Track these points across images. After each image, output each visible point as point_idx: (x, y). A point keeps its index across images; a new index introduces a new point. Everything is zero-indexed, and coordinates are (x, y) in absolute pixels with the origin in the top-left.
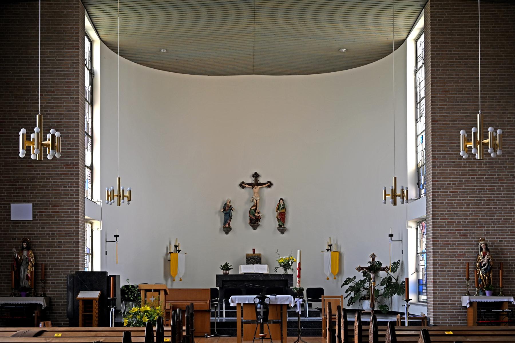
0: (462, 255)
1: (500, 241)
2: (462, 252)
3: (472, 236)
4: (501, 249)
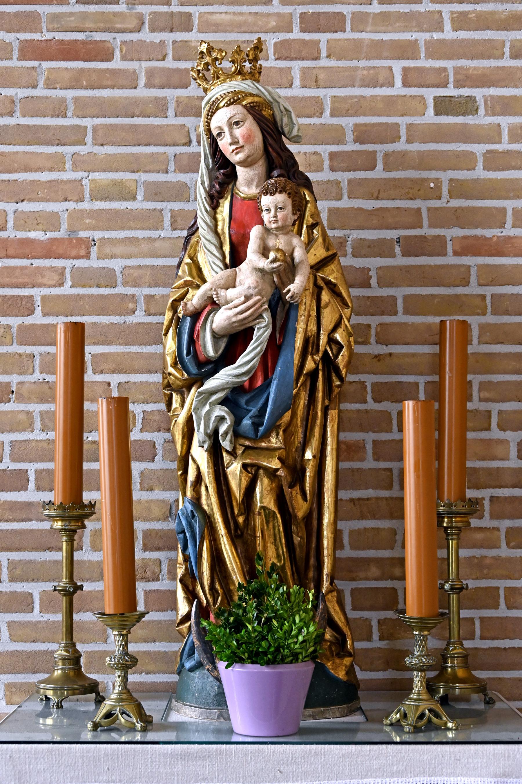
0: (49, 250)
1: (443, 106)
2: (51, 221)
3: (158, 52)
4: (458, 189)
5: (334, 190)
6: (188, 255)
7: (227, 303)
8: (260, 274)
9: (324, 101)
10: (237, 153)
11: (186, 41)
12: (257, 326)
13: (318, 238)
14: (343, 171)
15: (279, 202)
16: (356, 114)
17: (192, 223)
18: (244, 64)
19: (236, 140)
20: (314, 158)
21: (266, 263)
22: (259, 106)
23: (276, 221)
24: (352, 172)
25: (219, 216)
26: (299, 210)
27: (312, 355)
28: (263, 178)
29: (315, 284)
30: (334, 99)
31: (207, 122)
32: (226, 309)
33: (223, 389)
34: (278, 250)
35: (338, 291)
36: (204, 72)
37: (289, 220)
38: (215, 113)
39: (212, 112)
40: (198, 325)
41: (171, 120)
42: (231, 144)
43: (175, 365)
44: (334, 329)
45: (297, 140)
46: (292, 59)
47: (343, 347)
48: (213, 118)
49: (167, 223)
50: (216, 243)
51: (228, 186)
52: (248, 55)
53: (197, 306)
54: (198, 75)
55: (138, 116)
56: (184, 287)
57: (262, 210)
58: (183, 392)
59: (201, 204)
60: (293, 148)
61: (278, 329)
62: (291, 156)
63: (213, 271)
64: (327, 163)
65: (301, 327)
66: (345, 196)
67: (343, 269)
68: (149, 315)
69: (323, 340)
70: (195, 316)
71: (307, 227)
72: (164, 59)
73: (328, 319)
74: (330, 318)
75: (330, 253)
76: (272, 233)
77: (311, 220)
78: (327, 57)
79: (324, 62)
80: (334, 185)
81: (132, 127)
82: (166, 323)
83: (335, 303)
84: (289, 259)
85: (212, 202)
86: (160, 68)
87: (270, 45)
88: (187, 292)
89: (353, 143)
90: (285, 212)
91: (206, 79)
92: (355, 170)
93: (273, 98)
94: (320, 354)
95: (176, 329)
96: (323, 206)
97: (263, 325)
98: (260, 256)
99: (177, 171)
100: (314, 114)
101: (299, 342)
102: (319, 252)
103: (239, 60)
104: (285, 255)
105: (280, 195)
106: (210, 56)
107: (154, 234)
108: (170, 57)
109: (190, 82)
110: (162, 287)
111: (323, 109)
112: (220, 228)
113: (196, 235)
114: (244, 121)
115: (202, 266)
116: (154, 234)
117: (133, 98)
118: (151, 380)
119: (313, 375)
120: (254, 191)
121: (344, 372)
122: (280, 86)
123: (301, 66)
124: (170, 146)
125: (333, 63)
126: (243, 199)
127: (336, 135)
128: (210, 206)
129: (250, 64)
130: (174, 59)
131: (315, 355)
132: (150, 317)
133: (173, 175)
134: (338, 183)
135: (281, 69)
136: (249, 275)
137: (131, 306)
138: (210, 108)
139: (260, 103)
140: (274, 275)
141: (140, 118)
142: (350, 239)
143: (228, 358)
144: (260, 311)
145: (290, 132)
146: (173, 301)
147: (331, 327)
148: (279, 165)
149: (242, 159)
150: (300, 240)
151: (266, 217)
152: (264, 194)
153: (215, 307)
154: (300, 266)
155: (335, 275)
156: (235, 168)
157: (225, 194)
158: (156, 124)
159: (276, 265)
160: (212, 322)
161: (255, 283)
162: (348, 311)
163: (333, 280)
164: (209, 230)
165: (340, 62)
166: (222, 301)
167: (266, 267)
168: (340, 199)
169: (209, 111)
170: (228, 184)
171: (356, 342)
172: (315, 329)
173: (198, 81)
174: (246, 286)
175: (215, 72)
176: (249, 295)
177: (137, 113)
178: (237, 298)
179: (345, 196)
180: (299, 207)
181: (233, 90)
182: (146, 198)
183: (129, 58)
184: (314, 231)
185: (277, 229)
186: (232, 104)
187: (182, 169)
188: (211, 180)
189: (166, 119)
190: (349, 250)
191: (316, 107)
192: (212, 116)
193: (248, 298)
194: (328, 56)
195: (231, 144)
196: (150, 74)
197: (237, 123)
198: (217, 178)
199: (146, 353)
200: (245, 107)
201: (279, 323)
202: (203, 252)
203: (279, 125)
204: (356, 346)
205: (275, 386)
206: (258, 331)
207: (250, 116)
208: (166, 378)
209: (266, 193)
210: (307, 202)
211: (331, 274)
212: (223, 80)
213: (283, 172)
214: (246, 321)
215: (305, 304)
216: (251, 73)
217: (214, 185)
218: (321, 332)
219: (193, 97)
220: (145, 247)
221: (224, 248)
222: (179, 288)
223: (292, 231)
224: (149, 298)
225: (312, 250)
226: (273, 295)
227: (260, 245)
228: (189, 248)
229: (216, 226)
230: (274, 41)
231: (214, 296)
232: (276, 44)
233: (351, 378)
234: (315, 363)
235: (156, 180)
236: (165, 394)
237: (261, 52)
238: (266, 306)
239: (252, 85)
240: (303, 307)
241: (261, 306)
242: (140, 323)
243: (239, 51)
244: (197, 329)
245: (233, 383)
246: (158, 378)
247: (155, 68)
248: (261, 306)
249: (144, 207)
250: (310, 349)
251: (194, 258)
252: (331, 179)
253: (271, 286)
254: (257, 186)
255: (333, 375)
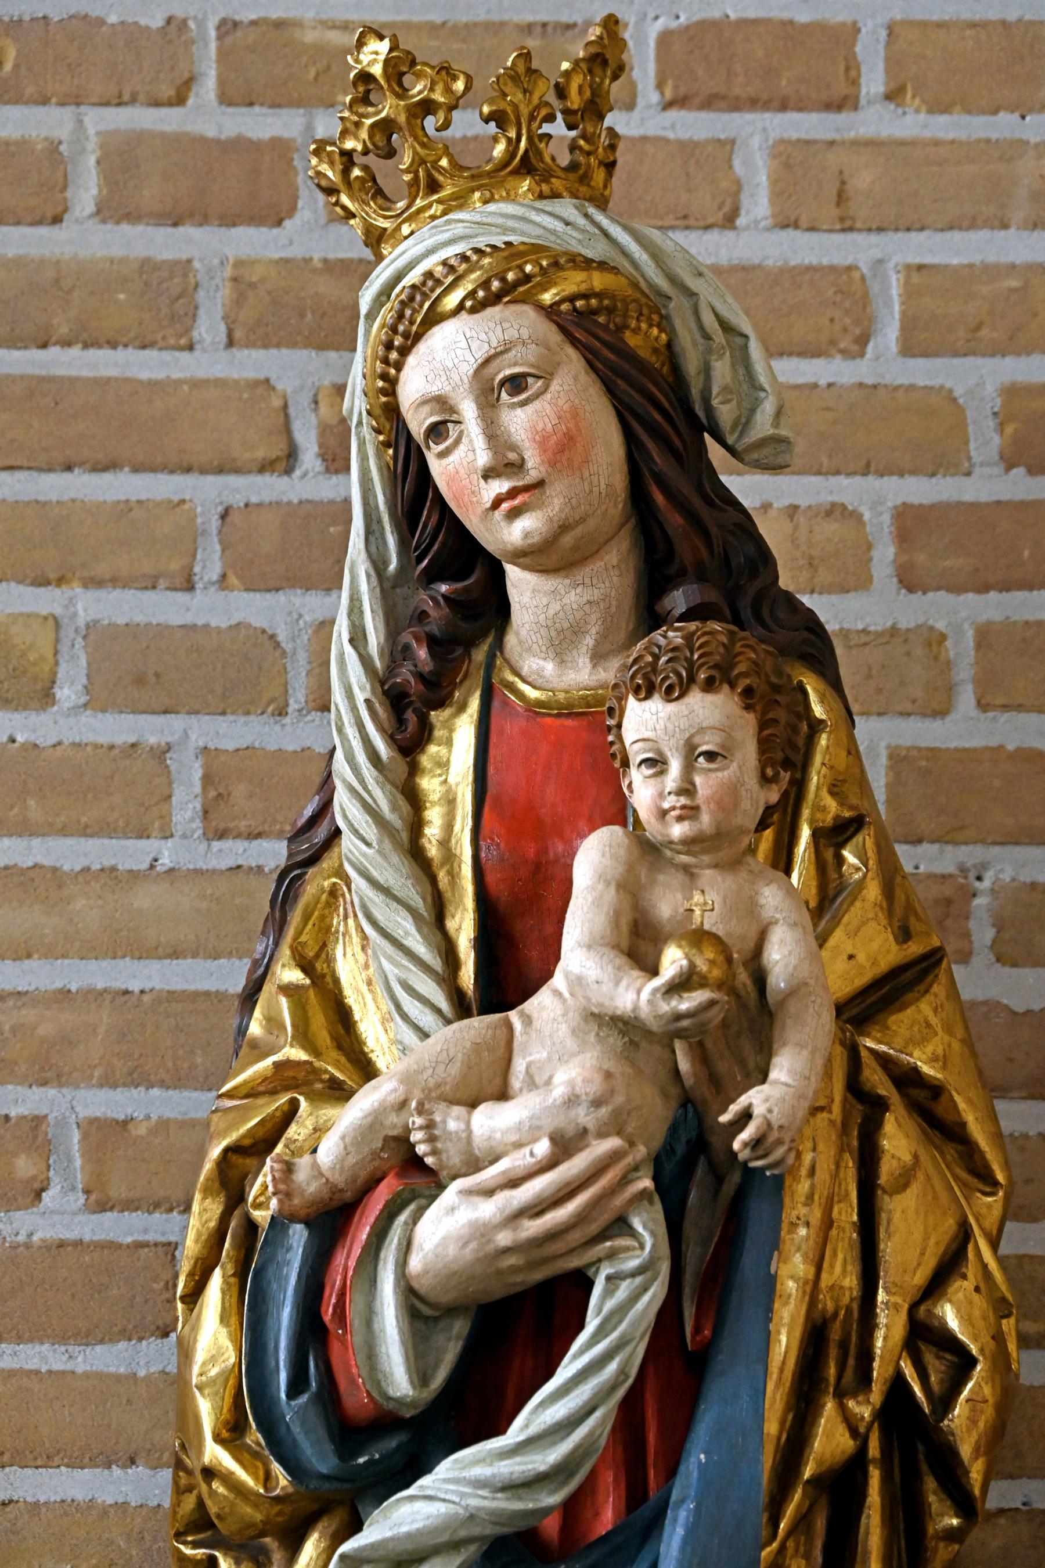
5: (921, 673)
6: (293, 950)
7: (474, 1164)
8: (616, 1041)
9: (875, 288)
10: (514, 514)
11: (280, 24)
12: (606, 1270)
13: (861, 884)
14: (956, 589)
15: (702, 730)
16: (1011, 345)
17: (308, 812)
18: (546, 128)
19: (512, 456)
20: (831, 528)
21: (645, 995)
22: (610, 311)
23: (690, 812)
24: (993, 595)
25: (429, 785)
26: (787, 764)
27: (840, 1395)
28: (625, 624)
29: (855, 1087)
30: (916, 279)
31: (384, 377)
32: (469, 1192)
33: (454, 1546)
34: (698, 938)
35: (950, 1118)
36: (371, 160)
37: (746, 805)
38: (418, 337)
39: (406, 335)
40: (339, 1259)
41: (211, 361)
42: (488, 474)
43: (231, 1433)
44: (936, 1286)
45: (771, 457)
46: (736, 105)
47: (974, 1362)
48: (411, 360)
49: (186, 804)
50: (418, 902)
51: (468, 654)
52: (561, 92)
53: (339, 1179)
54: (346, 172)
55: (67, 344)
56: (273, 1093)
57: (626, 763)
58: (265, 1551)
59: (351, 732)
60: (745, 486)
61: (689, 1278)
62: (743, 524)
63: (400, 1025)
64: (884, 554)
65: (792, 1272)
66: (966, 699)
67: (968, 1020)
68: (103, 1206)
69: (888, 1332)
70: (331, 1219)
71: (815, 834)
72: (180, 100)
73: (910, 1238)
74: (917, 1236)
75: (915, 949)
76: (671, 862)
77: (831, 804)
78: (889, 97)
79: (874, 120)
80: (919, 651)
81: (39, 386)
82: (191, 1246)
83: (938, 1169)
84: (743, 977)
85: (400, 721)
86: (163, 135)
87: (642, 42)
88: (290, 1113)
89: (998, 470)
90: (726, 774)
91: (379, 193)
92: (1006, 587)
93: (673, 279)
94: (876, 1395)
95: (241, 1273)
96: (876, 736)
97: (633, 1264)
98: (621, 960)
99: (233, 580)
100: (832, 342)
101: (784, 1339)
102: (866, 946)
103: (525, 111)
104: (729, 960)
105: (710, 698)
106: (402, 92)
107: (130, 854)
108: (208, 87)
109: (295, 198)
110: (163, 1085)
111: (871, 320)
112: (432, 832)
113: (327, 863)
114: (546, 376)
115: (351, 999)
116: (130, 854)
117: (42, 263)
118: (108, 1497)
119: (843, 1486)
120: (581, 675)
121: (976, 1473)
122: (686, 221)
123: (774, 135)
124: (203, 471)
125: (912, 124)
126: (533, 708)
127: (928, 435)
128: (391, 739)
129: (570, 127)
130: (226, 99)
131: (854, 1395)
132: (109, 1218)
133: (216, 596)
134: (934, 640)
135: (688, 149)
136: (571, 1044)
137: (24, 1166)
138: (401, 316)
139: (613, 297)
140: (679, 1046)
141: (75, 351)
142: (986, 884)
143: (471, 1405)
144: (619, 1201)
145: (744, 423)
146: (227, 1150)
147: (920, 1277)
148: (694, 564)
149: (536, 539)
150: (790, 890)
151: (643, 792)
152: (637, 690)
153: (418, 1181)
154: (792, 1007)
155: (936, 1045)
156: (502, 573)
157: (454, 686)
158: (144, 375)
159: (686, 1003)
160: (407, 1246)
161: (598, 1078)
162: (991, 1204)
163: (926, 1069)
164: (387, 845)
165: (943, 119)
166: (454, 1157)
167: (645, 1011)
168: (941, 713)
169: (394, 329)
170: (470, 643)
171: (1025, 1341)
172: (852, 1282)
173: (345, 199)
174: (559, 1091)
175: (419, 161)
176: (571, 1131)
177: (64, 330)
178: (518, 1145)
179: (966, 699)
180: (786, 749)
181: (498, 241)
182: (99, 698)
183: (30, 90)
184: (846, 853)
185: (690, 843)
186: (494, 299)
187: (250, 572)
188: (393, 628)
189: (185, 356)
190: (983, 933)
191: (841, 312)
192: (405, 351)
193: (564, 1146)
194: (894, 95)
195: (488, 474)
196: (122, 160)
197: (516, 383)
198: (422, 616)
199: (86, 1375)
200: (550, 312)
201: (694, 1256)
202: (356, 939)
203: (695, 392)
204: (1025, 1355)
205: (680, 1531)
206: (608, 1293)
207: (570, 351)
208: (190, 1489)
209: (646, 690)
210: (816, 726)
211: (919, 1040)
212: (455, 197)
213: (713, 596)
214: (559, 1246)
215: (812, 1172)
216: (573, 167)
217: (407, 648)
218: (881, 1296)
219: (308, 261)
220: (87, 910)
221: (451, 925)
222: (251, 1092)
223: (752, 850)
224: (106, 1135)
225: (838, 937)
226: (674, 1130)
227: (617, 915)
228: (295, 918)
229: (416, 826)
230: (660, 24)
231: (416, 1136)
232: (665, 39)
233: (1001, 1495)
234: (854, 1432)
235: (140, 619)
236: (182, 1558)
237: (615, 77)
238: (646, 1183)
239: (582, 221)
240: (803, 1187)
241: (625, 1181)
242: (62, 1245)
243: (525, 73)
244: (335, 1280)
245: (497, 1517)
246: (149, 1487)
247: (138, 138)
248: (625, 1181)
249: (89, 737)
250: (832, 1371)
251: (320, 966)
252: (903, 625)
253: (665, 1094)
254: (598, 657)
255: (930, 1484)
